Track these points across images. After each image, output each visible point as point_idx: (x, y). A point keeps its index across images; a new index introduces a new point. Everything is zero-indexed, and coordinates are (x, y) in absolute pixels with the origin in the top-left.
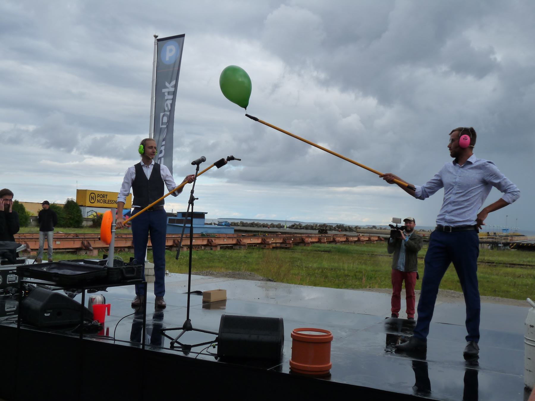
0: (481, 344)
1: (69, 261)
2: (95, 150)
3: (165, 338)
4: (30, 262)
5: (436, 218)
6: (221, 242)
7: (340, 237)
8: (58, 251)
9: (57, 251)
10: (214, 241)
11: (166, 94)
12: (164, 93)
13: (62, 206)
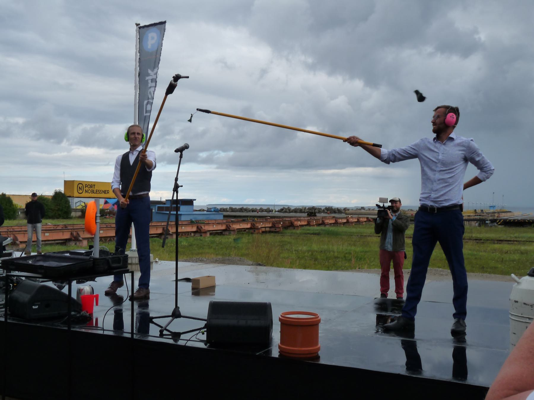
0: (468, 321)
1: (54, 253)
2: (85, 141)
3: (153, 325)
4: (17, 254)
5: (419, 196)
6: (211, 228)
7: (329, 219)
8: (47, 243)
9: (46, 242)
10: (203, 227)
11: (150, 81)
12: (148, 80)
13: (50, 198)
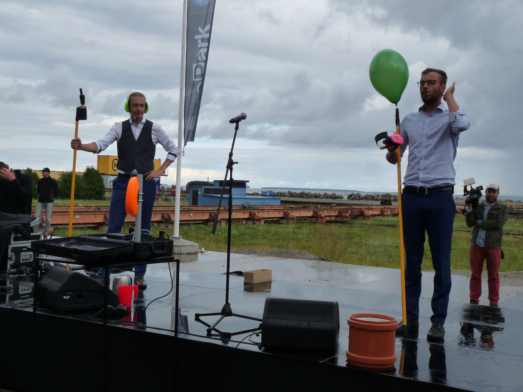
6: (265, 215)
9: (77, 226)
10: (256, 213)
11: (200, 41)
12: (197, 40)
13: (81, 175)
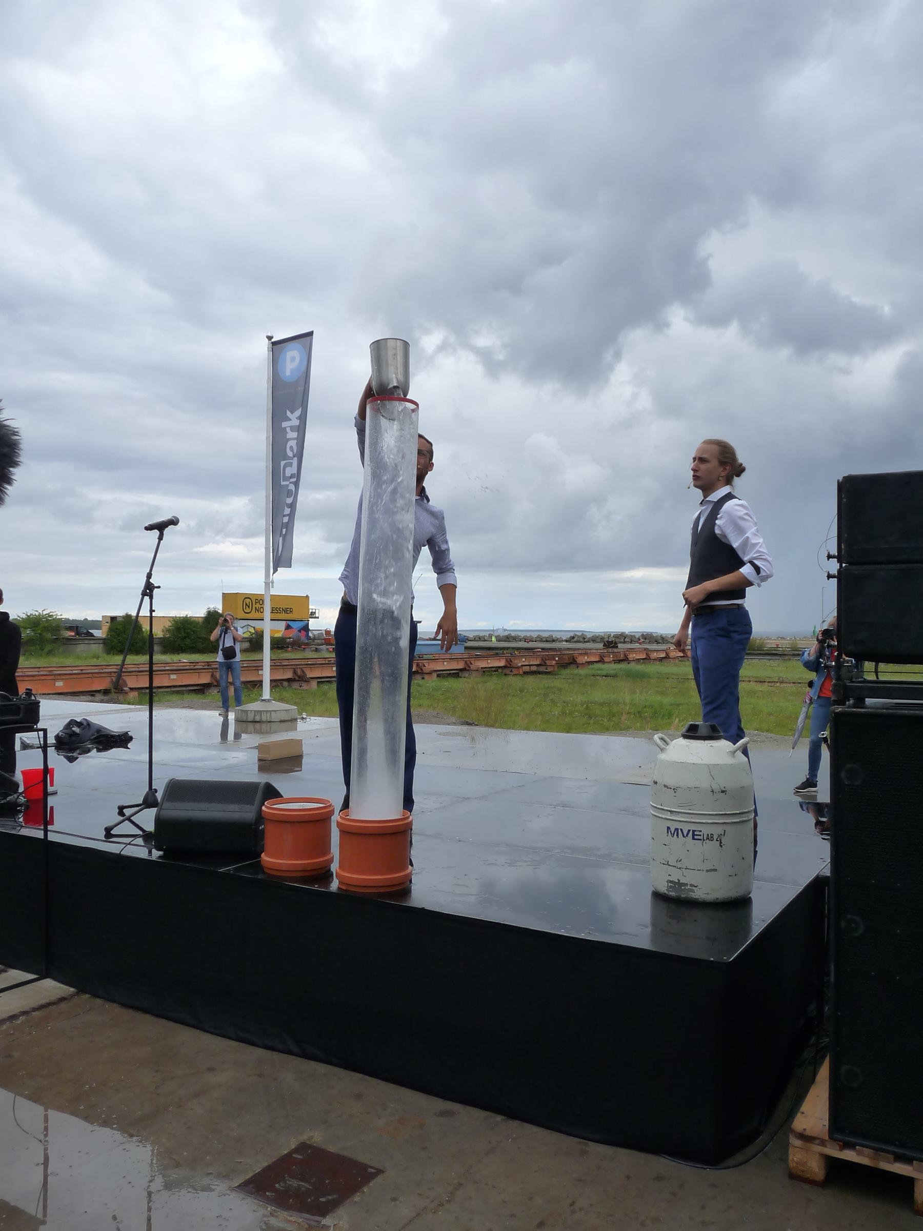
6: (439, 667)
